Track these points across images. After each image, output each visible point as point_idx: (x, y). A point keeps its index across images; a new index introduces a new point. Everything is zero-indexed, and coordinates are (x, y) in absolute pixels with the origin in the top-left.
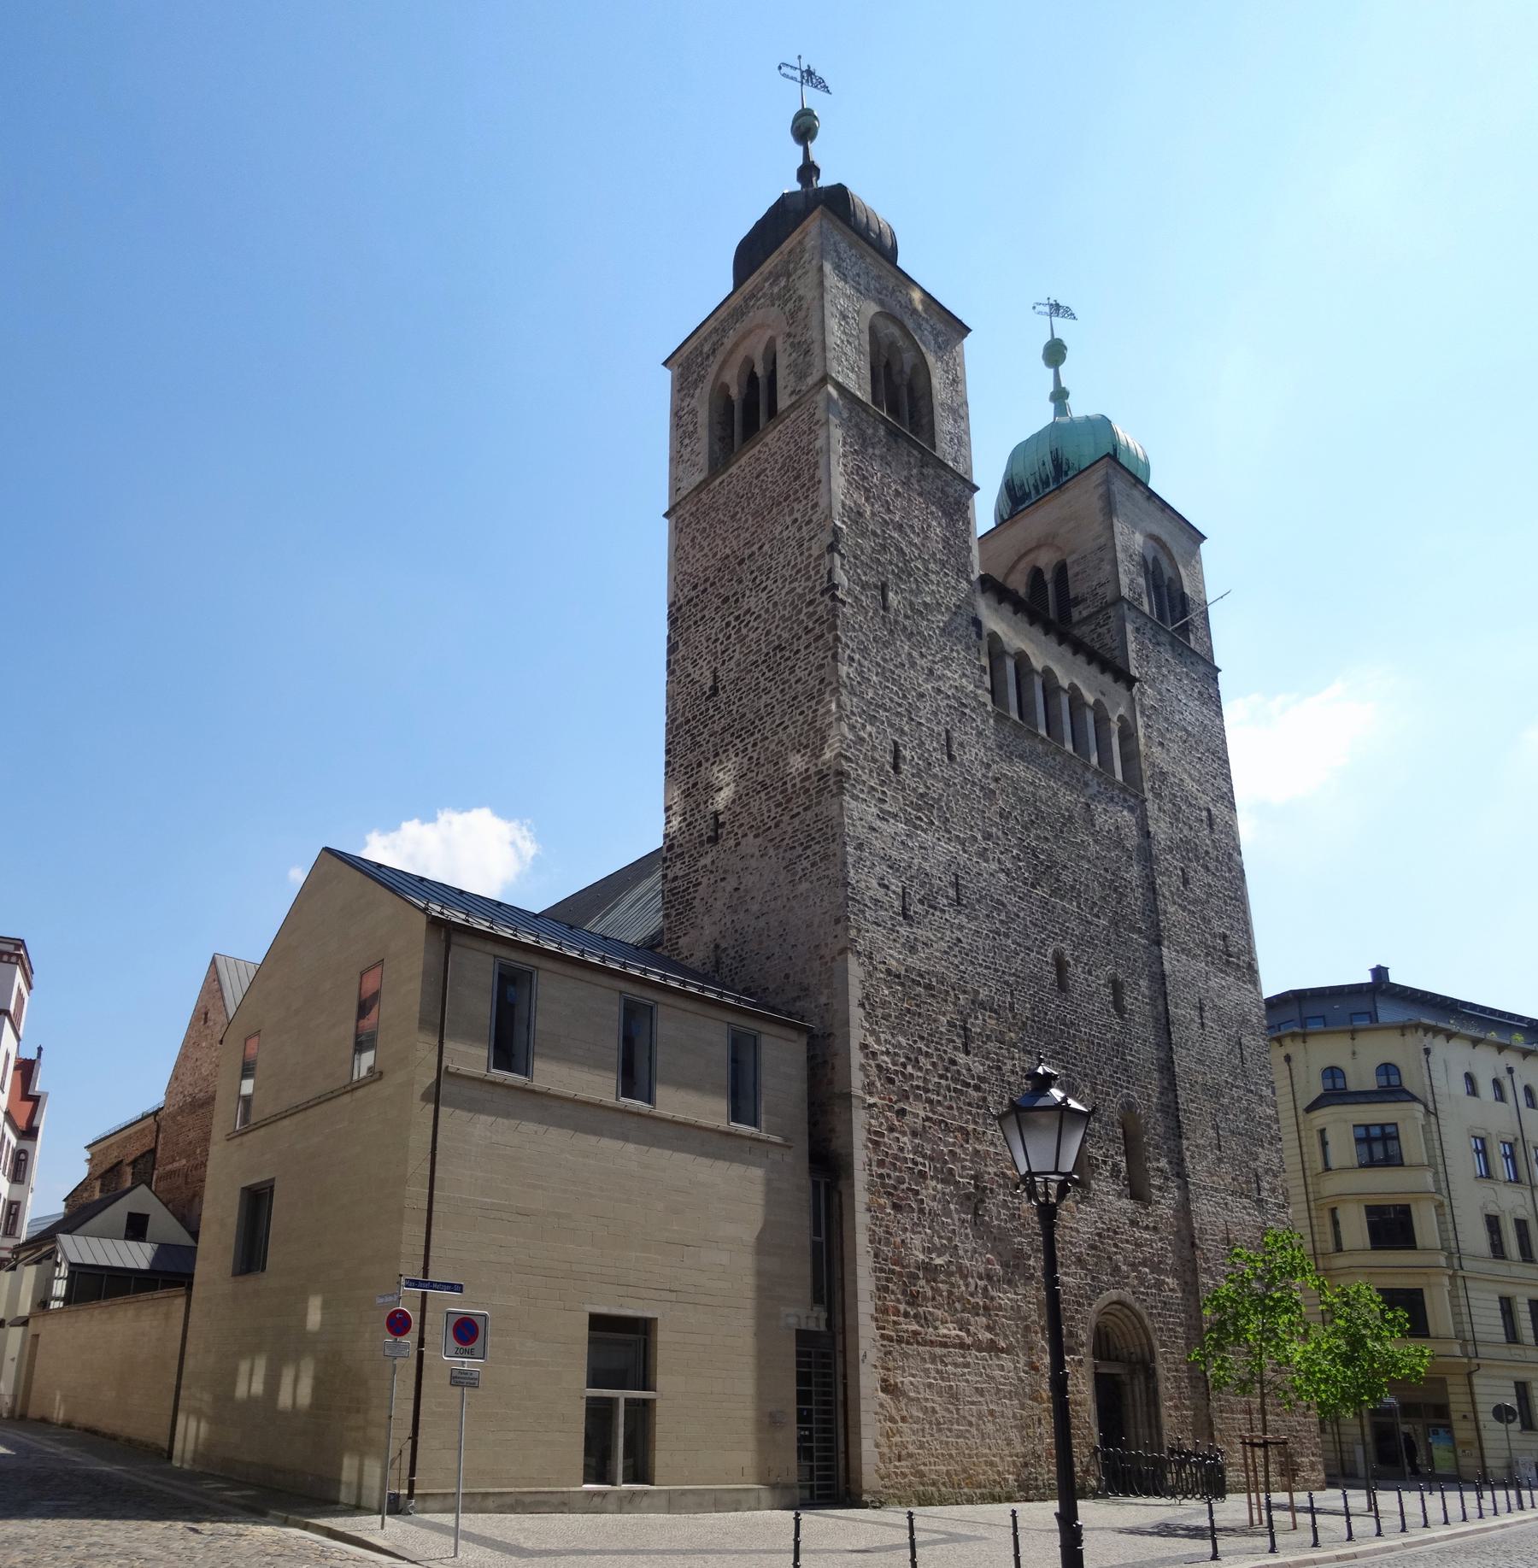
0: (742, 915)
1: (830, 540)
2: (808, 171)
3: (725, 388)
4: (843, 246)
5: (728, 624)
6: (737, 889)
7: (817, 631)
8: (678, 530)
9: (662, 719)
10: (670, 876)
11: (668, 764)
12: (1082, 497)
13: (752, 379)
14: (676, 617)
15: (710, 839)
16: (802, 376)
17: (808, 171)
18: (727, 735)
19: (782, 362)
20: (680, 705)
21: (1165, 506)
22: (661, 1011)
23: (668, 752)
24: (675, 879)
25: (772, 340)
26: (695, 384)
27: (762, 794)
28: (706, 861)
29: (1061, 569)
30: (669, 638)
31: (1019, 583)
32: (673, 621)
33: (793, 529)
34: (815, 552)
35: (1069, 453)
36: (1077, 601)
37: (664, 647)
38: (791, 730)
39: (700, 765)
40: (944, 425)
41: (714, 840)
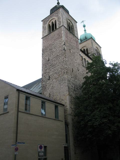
0: (53, 90)
1: (64, 43)
2: (58, 3)
3: (49, 25)
4: (64, 12)
5: (50, 52)
6: (52, 86)
7: (63, 54)
8: (43, 40)
9: (41, 63)
10: (43, 84)
11: (42, 69)
12: (89, 42)
13: (53, 24)
14: (43, 51)
15: (48, 79)
16: (60, 25)
17: (58, 3)
18: (51, 66)
19: (57, 23)
20: (44, 62)
21: (97, 44)
22: (46, 103)
23: (42, 68)
24: (43, 84)
25: (56, 20)
26: (46, 24)
27: (56, 74)
28: (48, 82)
29: (87, 49)
30: (42, 53)
31: (83, 50)
32: (43, 51)
33: (59, 42)
34: (62, 45)
35: (87, 37)
36: (89, 53)
37: (42, 54)
38: (60, 66)
39: (47, 69)
40: (75, 32)
41: (49, 79)
